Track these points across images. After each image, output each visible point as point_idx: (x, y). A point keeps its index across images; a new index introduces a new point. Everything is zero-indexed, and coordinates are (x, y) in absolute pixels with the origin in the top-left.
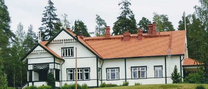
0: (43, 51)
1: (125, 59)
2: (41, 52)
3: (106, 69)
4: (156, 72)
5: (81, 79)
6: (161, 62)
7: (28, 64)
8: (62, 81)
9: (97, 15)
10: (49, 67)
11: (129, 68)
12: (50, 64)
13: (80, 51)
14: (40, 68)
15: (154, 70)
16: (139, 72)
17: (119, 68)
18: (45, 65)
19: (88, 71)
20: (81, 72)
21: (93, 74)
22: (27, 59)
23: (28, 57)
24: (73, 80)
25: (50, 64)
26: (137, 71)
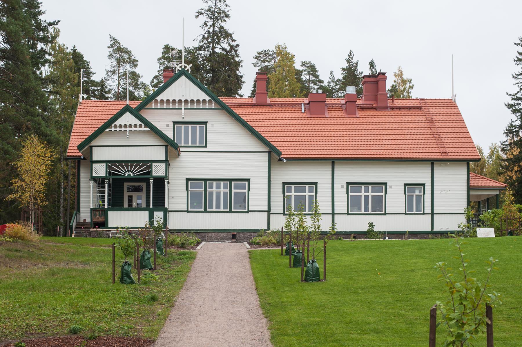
0: (138, 129)
1: (333, 162)
2: (133, 129)
3: (185, 182)
4: (409, 201)
6: (420, 175)
7: (94, 159)
9: (111, 37)
10: (150, 173)
11: (342, 187)
12: (154, 165)
13: (222, 131)
14: (126, 175)
16: (218, 193)
17: (316, 184)
18: (141, 167)
21: (257, 198)
22: (91, 147)
23: (93, 144)
24: (228, 210)
26: (363, 193)
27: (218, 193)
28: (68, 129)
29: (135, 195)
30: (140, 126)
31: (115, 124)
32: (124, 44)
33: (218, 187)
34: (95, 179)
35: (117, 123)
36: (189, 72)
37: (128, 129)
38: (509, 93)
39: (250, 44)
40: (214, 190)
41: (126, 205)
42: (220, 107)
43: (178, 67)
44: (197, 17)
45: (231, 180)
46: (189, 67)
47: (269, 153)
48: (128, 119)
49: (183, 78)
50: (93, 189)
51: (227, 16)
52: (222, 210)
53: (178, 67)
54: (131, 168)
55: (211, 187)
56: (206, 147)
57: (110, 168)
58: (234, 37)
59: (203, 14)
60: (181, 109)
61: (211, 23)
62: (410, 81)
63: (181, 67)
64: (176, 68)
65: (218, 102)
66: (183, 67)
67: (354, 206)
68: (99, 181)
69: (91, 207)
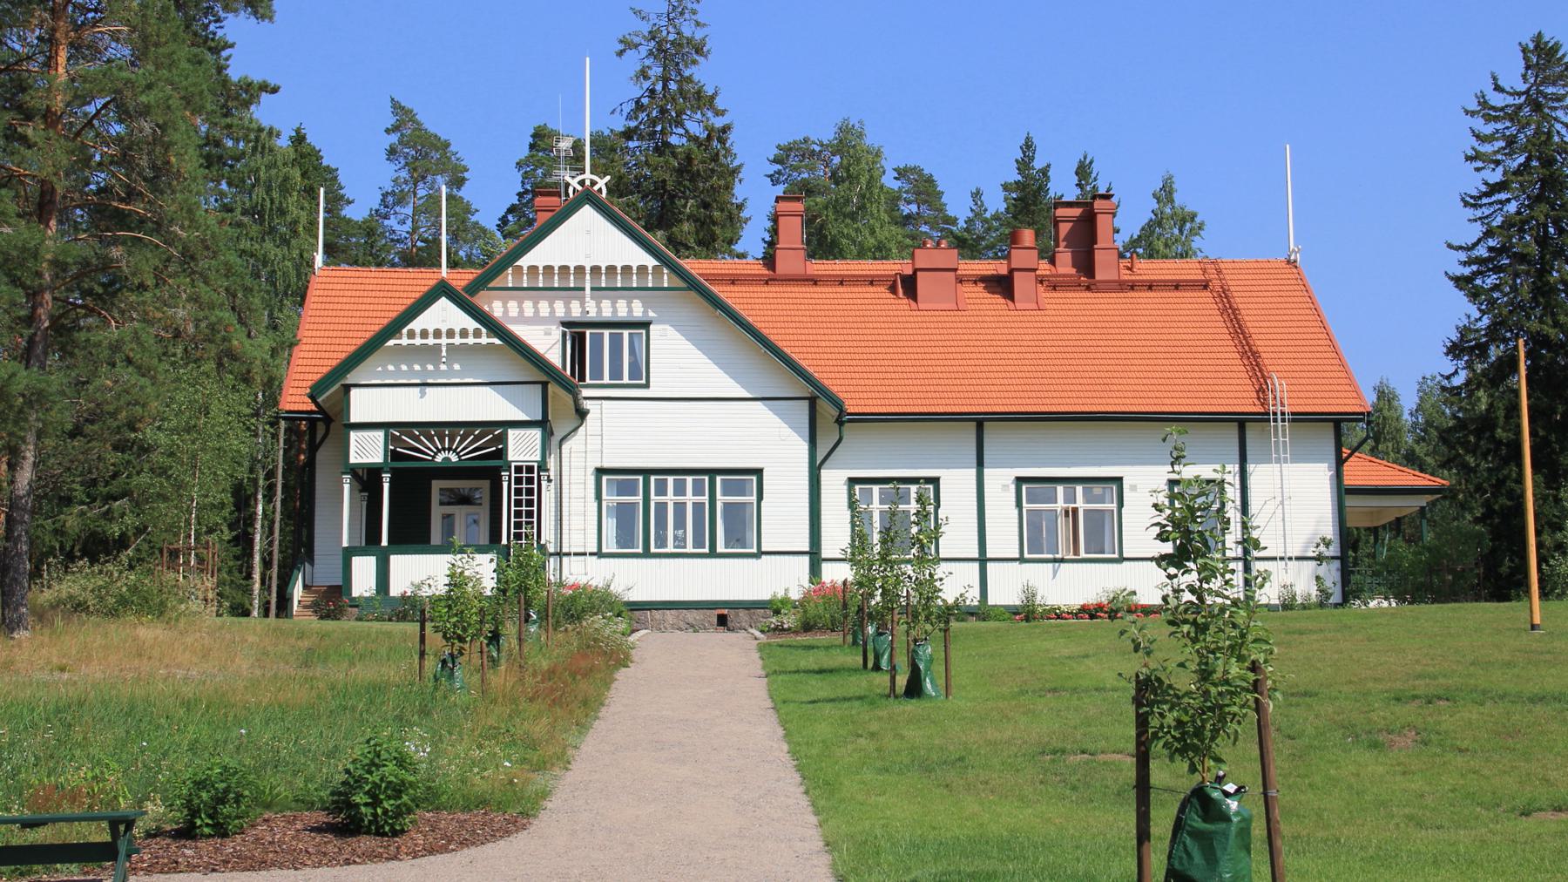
0: (471, 340)
2: (457, 340)
3: (1013, 488)
5: (698, 542)
8: (560, 554)
10: (500, 454)
12: (511, 433)
14: (439, 458)
15: (1019, 504)
16: (680, 508)
19: (635, 494)
20: (699, 499)
21: (783, 519)
22: (347, 388)
23: (351, 378)
24: (707, 550)
25: (511, 433)
27: (680, 508)
28: (286, 346)
29: (460, 512)
30: (477, 334)
31: (410, 326)
32: (433, 122)
33: (680, 490)
34: (354, 471)
35: (417, 325)
36: (604, 195)
37: (444, 341)
38: (1456, 243)
39: (760, 118)
40: (670, 498)
41: (436, 538)
42: (682, 284)
43: (574, 183)
44: (620, 53)
45: (713, 472)
46: (602, 183)
47: (812, 401)
48: (444, 315)
49: (587, 211)
50: (351, 498)
51: (699, 51)
52: (690, 549)
53: (574, 183)
54: (452, 441)
55: (661, 490)
56: (647, 386)
57: (396, 440)
58: (720, 103)
59: (637, 46)
60: (583, 289)
61: (656, 71)
62: (1193, 217)
63: (582, 183)
64: (567, 185)
65: (677, 271)
66: (588, 183)
67: (1036, 543)
68: (367, 479)
69: (345, 544)
